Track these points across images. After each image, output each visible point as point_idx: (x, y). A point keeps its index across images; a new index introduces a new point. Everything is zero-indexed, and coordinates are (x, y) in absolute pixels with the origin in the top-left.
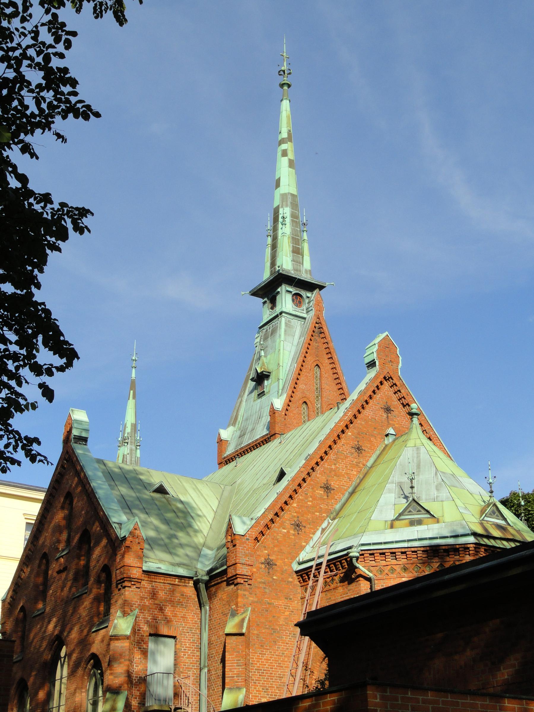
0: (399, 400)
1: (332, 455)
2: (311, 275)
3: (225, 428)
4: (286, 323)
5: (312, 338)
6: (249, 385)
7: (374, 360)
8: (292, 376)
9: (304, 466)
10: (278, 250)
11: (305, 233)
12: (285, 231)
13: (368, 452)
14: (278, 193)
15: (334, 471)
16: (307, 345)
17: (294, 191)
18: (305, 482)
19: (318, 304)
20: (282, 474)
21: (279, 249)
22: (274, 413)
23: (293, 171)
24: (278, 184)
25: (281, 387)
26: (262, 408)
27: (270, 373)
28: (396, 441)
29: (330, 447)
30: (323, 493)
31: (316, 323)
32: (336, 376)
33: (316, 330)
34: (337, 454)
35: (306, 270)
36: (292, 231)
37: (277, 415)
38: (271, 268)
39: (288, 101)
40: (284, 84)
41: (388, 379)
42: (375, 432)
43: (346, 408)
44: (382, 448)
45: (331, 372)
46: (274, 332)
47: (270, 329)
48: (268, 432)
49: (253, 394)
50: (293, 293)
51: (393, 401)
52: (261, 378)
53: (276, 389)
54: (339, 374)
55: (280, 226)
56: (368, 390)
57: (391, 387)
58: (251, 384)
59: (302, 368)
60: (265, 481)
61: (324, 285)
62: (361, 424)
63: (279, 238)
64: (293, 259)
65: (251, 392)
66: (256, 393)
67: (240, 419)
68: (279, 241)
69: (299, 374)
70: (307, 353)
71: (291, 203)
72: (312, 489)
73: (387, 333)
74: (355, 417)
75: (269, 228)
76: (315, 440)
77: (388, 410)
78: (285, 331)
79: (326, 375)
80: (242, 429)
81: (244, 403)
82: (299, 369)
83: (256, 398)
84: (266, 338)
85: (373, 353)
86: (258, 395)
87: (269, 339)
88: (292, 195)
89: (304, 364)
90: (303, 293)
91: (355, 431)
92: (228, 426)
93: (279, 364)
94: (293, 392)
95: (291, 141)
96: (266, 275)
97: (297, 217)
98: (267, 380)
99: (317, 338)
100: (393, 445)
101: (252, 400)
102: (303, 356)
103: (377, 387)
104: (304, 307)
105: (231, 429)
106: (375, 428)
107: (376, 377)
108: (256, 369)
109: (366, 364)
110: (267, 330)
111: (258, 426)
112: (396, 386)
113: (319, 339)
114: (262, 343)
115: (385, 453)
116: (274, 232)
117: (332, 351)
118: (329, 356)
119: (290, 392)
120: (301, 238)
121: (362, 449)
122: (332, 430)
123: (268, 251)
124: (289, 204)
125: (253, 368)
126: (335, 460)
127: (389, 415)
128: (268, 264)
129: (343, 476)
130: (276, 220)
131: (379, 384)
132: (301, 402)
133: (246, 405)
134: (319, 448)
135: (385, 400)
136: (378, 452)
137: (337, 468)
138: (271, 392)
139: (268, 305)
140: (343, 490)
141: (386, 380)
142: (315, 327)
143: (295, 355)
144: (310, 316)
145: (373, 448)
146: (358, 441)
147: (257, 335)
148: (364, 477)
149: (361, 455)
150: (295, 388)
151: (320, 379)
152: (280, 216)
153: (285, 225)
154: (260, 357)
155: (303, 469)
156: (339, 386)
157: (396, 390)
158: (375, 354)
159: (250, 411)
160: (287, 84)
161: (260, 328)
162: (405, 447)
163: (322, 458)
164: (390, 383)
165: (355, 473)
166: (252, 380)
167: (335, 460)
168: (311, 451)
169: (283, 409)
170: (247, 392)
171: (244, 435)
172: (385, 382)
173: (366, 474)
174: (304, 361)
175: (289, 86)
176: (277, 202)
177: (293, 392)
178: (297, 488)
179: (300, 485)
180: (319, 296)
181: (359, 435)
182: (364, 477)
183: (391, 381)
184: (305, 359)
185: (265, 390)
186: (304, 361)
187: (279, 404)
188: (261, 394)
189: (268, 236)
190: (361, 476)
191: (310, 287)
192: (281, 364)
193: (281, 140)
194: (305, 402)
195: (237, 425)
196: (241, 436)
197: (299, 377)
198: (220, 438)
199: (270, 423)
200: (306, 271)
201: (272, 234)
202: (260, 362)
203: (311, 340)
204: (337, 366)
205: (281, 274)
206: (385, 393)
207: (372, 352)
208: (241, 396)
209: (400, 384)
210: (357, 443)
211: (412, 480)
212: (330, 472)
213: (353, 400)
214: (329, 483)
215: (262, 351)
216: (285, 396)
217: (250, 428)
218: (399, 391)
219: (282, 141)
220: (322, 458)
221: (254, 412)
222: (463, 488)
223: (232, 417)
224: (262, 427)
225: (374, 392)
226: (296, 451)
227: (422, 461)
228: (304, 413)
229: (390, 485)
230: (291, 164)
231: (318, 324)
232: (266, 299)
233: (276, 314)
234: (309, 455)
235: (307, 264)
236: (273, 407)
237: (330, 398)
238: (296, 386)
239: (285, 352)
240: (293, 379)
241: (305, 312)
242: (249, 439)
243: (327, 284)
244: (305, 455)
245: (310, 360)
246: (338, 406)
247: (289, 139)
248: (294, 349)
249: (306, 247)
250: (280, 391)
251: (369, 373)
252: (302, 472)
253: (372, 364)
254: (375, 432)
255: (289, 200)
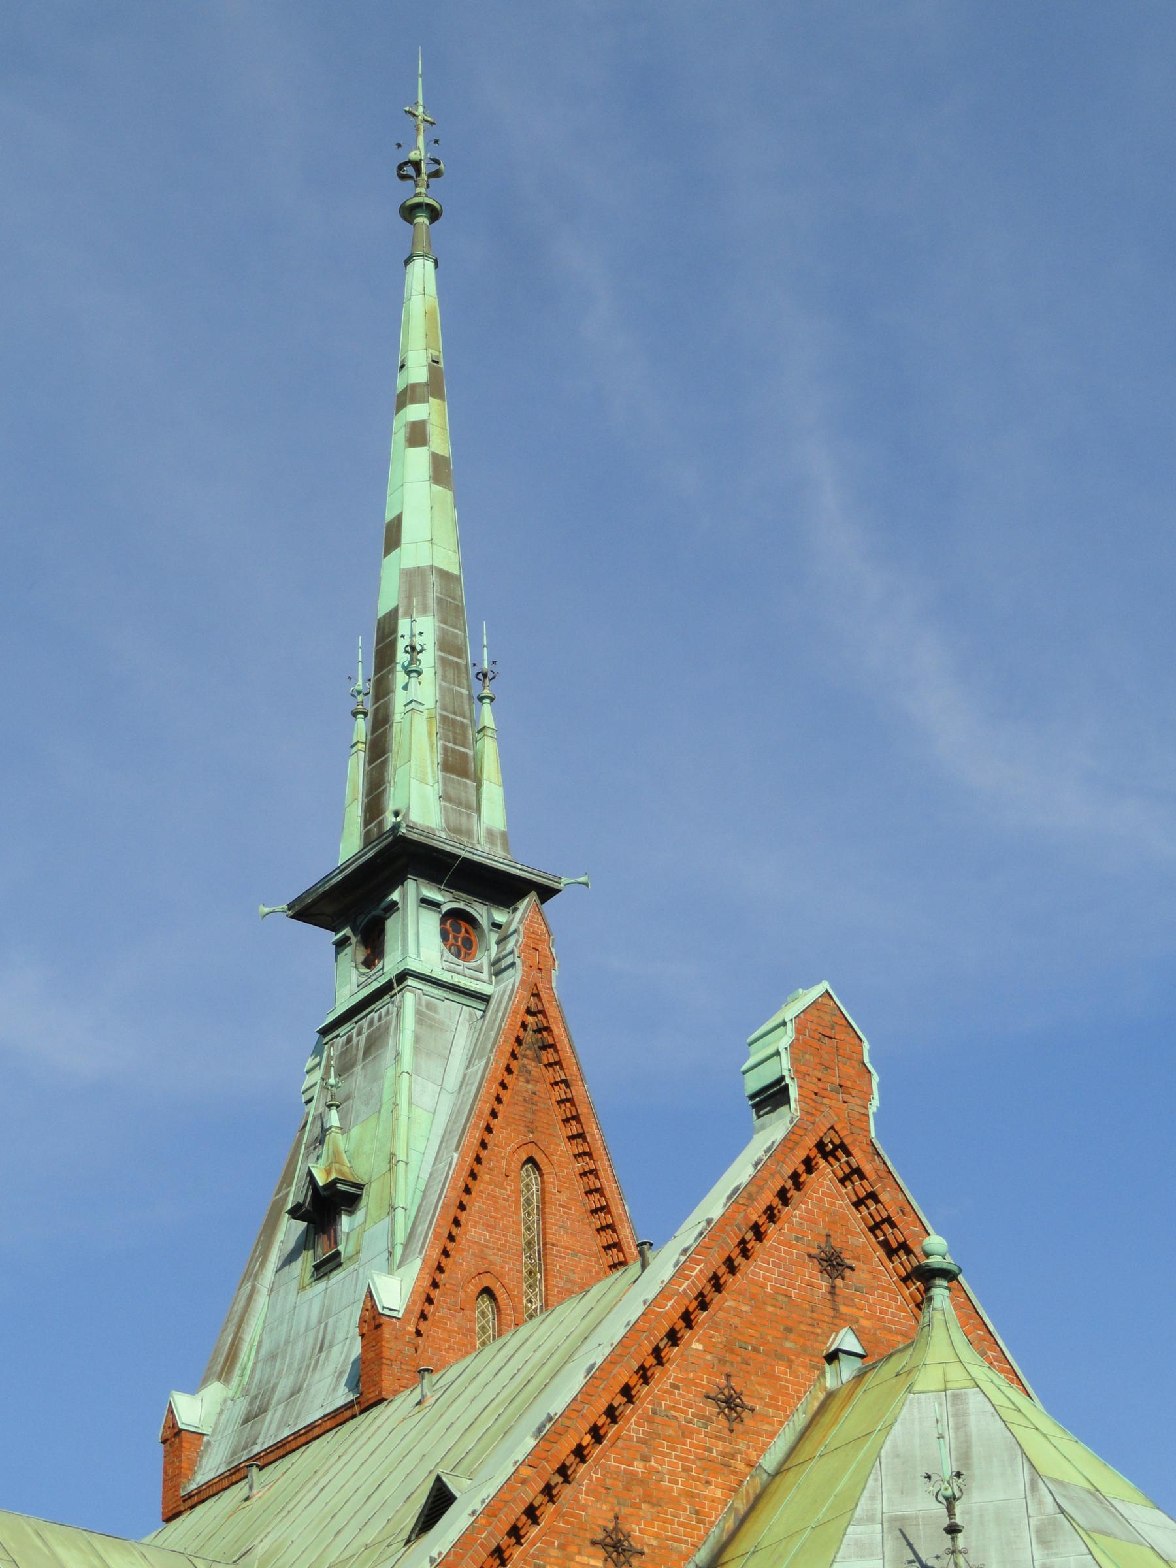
0: (872, 1230)
1: (632, 1426)
2: (506, 846)
3: (192, 1389)
4: (418, 1012)
5: (514, 1065)
6: (280, 1236)
7: (782, 1078)
8: (442, 1194)
9: (532, 1460)
10: (392, 763)
11: (487, 706)
12: (419, 695)
13: (766, 1418)
14: (392, 568)
15: (642, 1482)
16: (495, 1088)
17: (450, 562)
18: (535, 1521)
19: (534, 945)
20: (440, 1501)
21: (395, 758)
22: (378, 1326)
23: (445, 495)
24: (393, 537)
25: (401, 1236)
26: (328, 1315)
27: (360, 1187)
28: (871, 1375)
29: (626, 1391)
30: (600, 1564)
31: (529, 1012)
32: (595, 1201)
33: (528, 1036)
34: (650, 1421)
35: (489, 828)
36: (443, 696)
37: (386, 1332)
38: (366, 823)
39: (430, 265)
40: (419, 206)
41: (832, 1153)
42: (788, 1344)
43: (685, 1251)
44: (816, 1404)
45: (579, 1186)
46: (374, 1043)
47: (359, 1034)
48: (351, 1397)
49: (297, 1265)
50: (445, 908)
51: (849, 1232)
52: (326, 1206)
53: (383, 1244)
54: (607, 1192)
55: (400, 677)
56: (760, 1188)
57: (842, 1181)
58: (290, 1230)
59: (477, 1168)
60: (369, 1536)
61: (555, 885)
62: (738, 1313)
63: (397, 717)
64: (445, 792)
65: (290, 1258)
66: (307, 1261)
67: (246, 1355)
68: (396, 729)
69: (467, 1190)
70: (494, 1114)
71: (440, 601)
72: (562, 1547)
73: (824, 986)
74: (717, 1283)
75: (360, 686)
76: (569, 1366)
77: (833, 1264)
78: (417, 1039)
79: (563, 1197)
80: (253, 1392)
81: (262, 1300)
82: (466, 1171)
83: (307, 1280)
84: (345, 1068)
85: (778, 1053)
86: (317, 1268)
87: (358, 1068)
88: (444, 575)
89: (484, 1154)
90: (481, 912)
91: (718, 1338)
92: (205, 1382)
93: (393, 1155)
94: (446, 1253)
95: (438, 394)
96: (350, 845)
97: (459, 651)
98: (351, 1213)
99: (531, 1065)
100: (860, 1391)
101: (294, 1285)
102: (482, 1124)
103: (795, 1176)
104: (483, 960)
105: (215, 1391)
106: (789, 1330)
107: (789, 1142)
108: (310, 1174)
109: (752, 1097)
110: (349, 1040)
111: (317, 1376)
112: (862, 1176)
113: (536, 1070)
114: (332, 1081)
115: (826, 1419)
116: (377, 698)
117: (583, 1110)
118: (574, 1129)
119: (436, 1253)
120: (474, 722)
121: (743, 1406)
122: (634, 1330)
123: (357, 766)
124: (432, 603)
125: (300, 1172)
126: (645, 1442)
127: (839, 1282)
128: (355, 811)
129: (676, 1502)
130: (385, 657)
131: (801, 1169)
132: (473, 1289)
133: (271, 1306)
134: (585, 1394)
135: (821, 1229)
136: (800, 1419)
137: (654, 1471)
138: (364, 1255)
139: (355, 952)
140: (675, 1557)
141: (825, 1156)
142: (524, 1026)
143: (452, 1121)
144: (505, 990)
145: (783, 1404)
146: (728, 1376)
147: (310, 1063)
148: (752, 1508)
149: (738, 1427)
150: (451, 1238)
151: (542, 1211)
152: (401, 644)
153: (419, 673)
154: (325, 1131)
155: (526, 1472)
156: (608, 1238)
157: (862, 1194)
158: (786, 1059)
159: (284, 1328)
160: (428, 205)
161: (325, 1032)
162: (910, 1390)
163: (596, 1434)
164: (838, 1167)
165: (718, 1493)
166: (295, 1213)
167: (645, 1442)
168: (558, 1402)
169: (408, 1311)
170: (274, 1258)
171: (263, 1410)
172: (822, 1163)
173: (758, 1498)
174: (484, 1145)
175: (434, 214)
176: (389, 597)
177: (446, 1253)
178: (505, 1541)
179: (515, 1533)
180: (538, 918)
181: (732, 1351)
182: (752, 1508)
183: (844, 1159)
184: (489, 1138)
185: (341, 1248)
186: (484, 1145)
187: (395, 1293)
188: (327, 1266)
189: (355, 714)
190: (742, 1507)
191: (503, 888)
192: (401, 1155)
193: (404, 391)
194: (487, 1291)
195: (235, 1380)
196: (252, 1417)
197: (466, 1199)
198: (175, 1425)
199: (361, 1361)
200: (490, 834)
201: (369, 706)
202: (326, 1151)
203: (509, 1070)
204: (602, 1165)
205: (404, 840)
206: (821, 1200)
207: (773, 1053)
208: (252, 1275)
209: (876, 1171)
210: (722, 1381)
211: (950, 1502)
212: (627, 1488)
213: (709, 1222)
214: (625, 1527)
215: (334, 1113)
216: (415, 1266)
217: (284, 1386)
218: (873, 1196)
219: (409, 395)
220: (596, 1434)
221: (300, 1324)
222: (1138, 1539)
223: (217, 1350)
224: (329, 1381)
225: (783, 1195)
226: (487, 1420)
227: (974, 1439)
228: (483, 1328)
229: (861, 1528)
230: (440, 471)
231: (533, 1014)
232: (347, 931)
233: (383, 980)
234: (550, 1419)
235: (493, 811)
236: (374, 1306)
237: (575, 1277)
238: (455, 1231)
239: (415, 1112)
240: (445, 1206)
241: (485, 976)
242: (283, 1423)
243: (564, 880)
244: (536, 1417)
245: (506, 1140)
246: (642, 1254)
247: (435, 386)
248: (446, 1105)
249: (489, 753)
250: (399, 1250)
251: (763, 1127)
252: (524, 1482)
253: (772, 1097)
254: (788, 1344)
255: (434, 591)
